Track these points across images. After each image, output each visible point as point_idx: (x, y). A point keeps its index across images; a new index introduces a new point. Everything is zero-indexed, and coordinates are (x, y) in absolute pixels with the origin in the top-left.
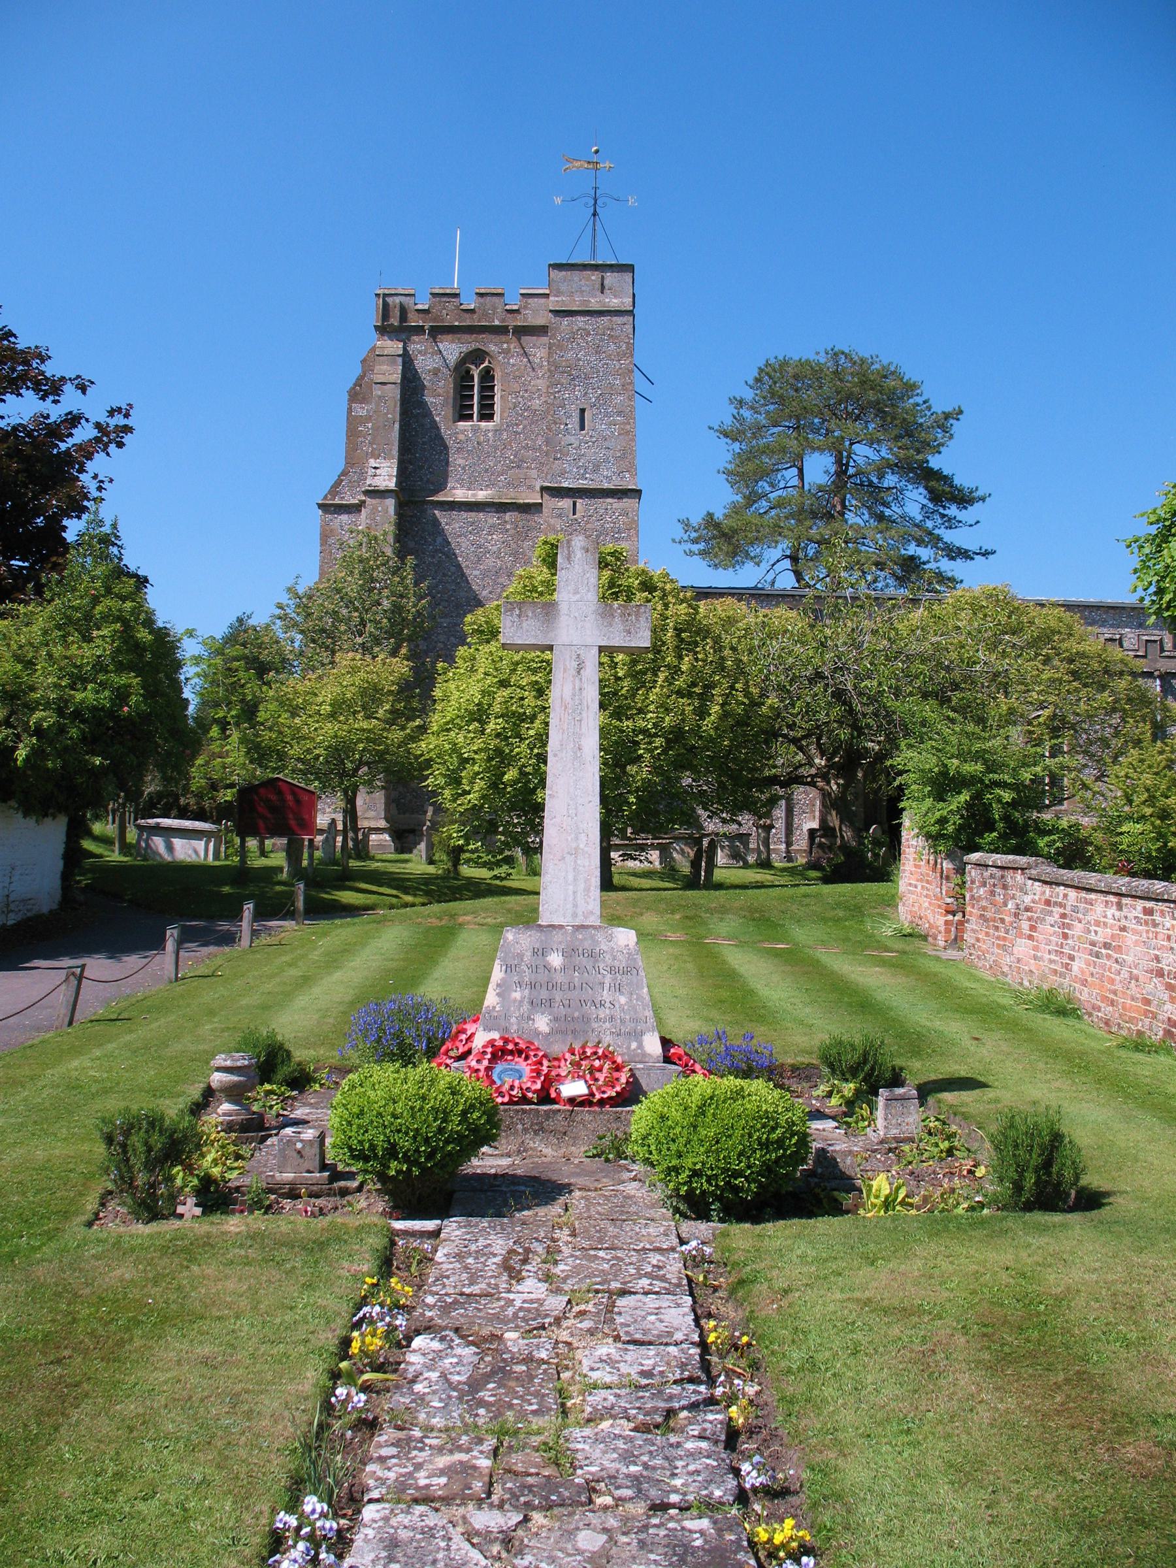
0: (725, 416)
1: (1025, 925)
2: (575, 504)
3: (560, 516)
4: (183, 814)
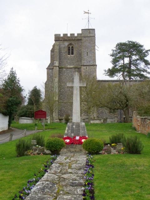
0: (111, 52)
1: (147, 126)
4: (26, 117)
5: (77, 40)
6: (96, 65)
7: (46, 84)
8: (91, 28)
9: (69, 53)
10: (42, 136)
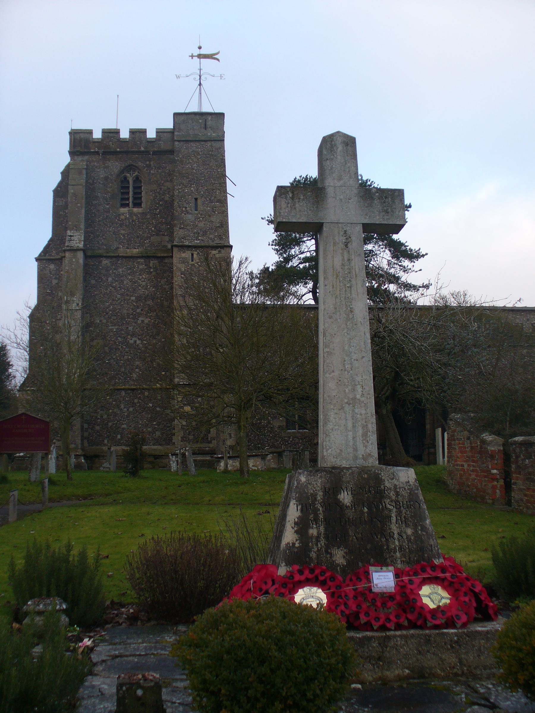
2: (192, 255)
3: (183, 262)
5: (155, 153)
6: (231, 247)
7: (31, 316)
8: (211, 111)
9: (123, 199)
10: (83, 555)
